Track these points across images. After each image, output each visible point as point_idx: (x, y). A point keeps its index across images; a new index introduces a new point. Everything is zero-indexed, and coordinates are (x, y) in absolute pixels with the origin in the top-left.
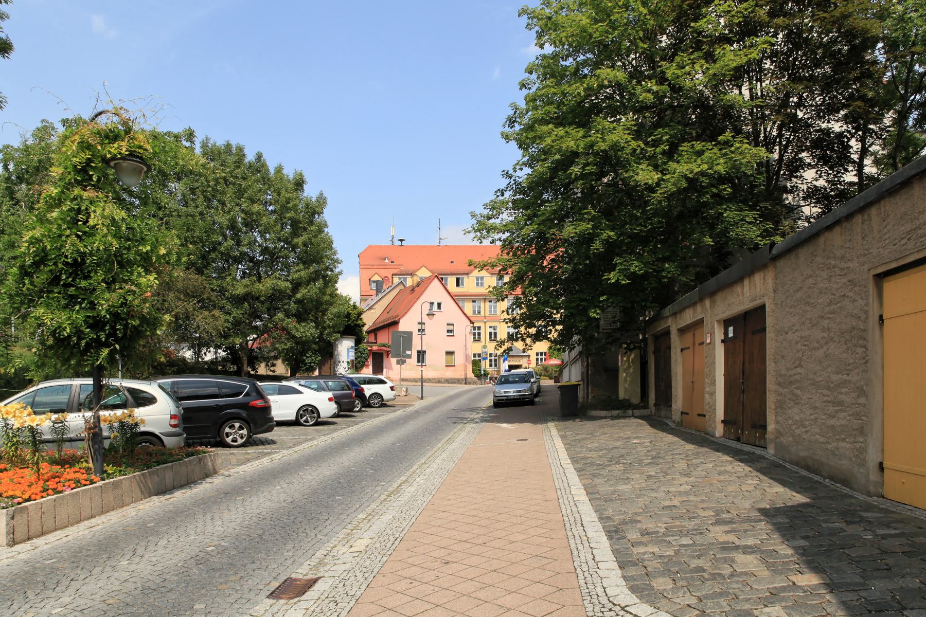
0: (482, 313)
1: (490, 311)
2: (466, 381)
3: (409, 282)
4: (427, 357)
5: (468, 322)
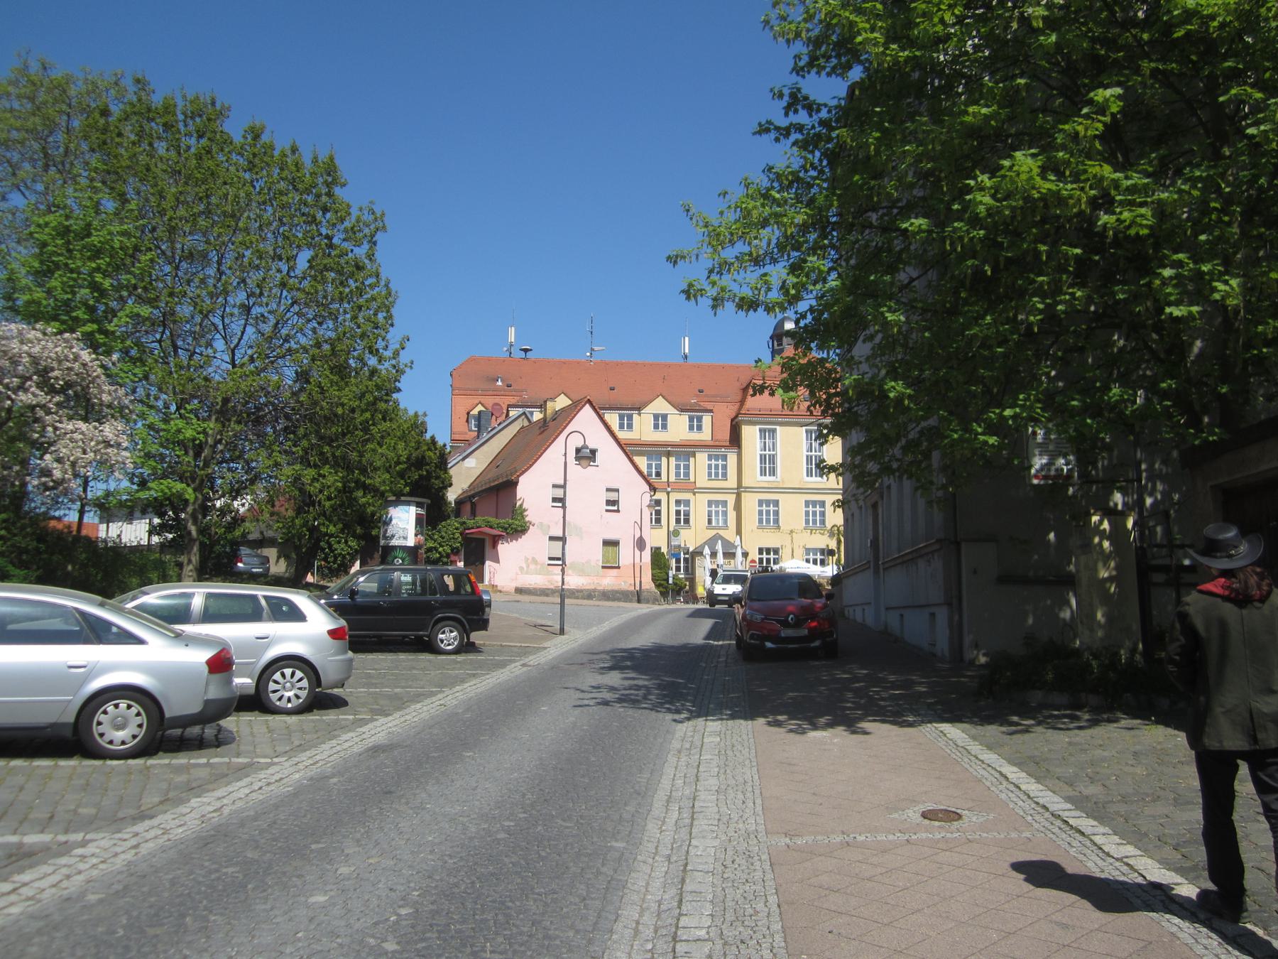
0: (664, 478)
1: (678, 474)
2: (639, 597)
3: (537, 416)
4: (611, 536)
5: (647, 488)
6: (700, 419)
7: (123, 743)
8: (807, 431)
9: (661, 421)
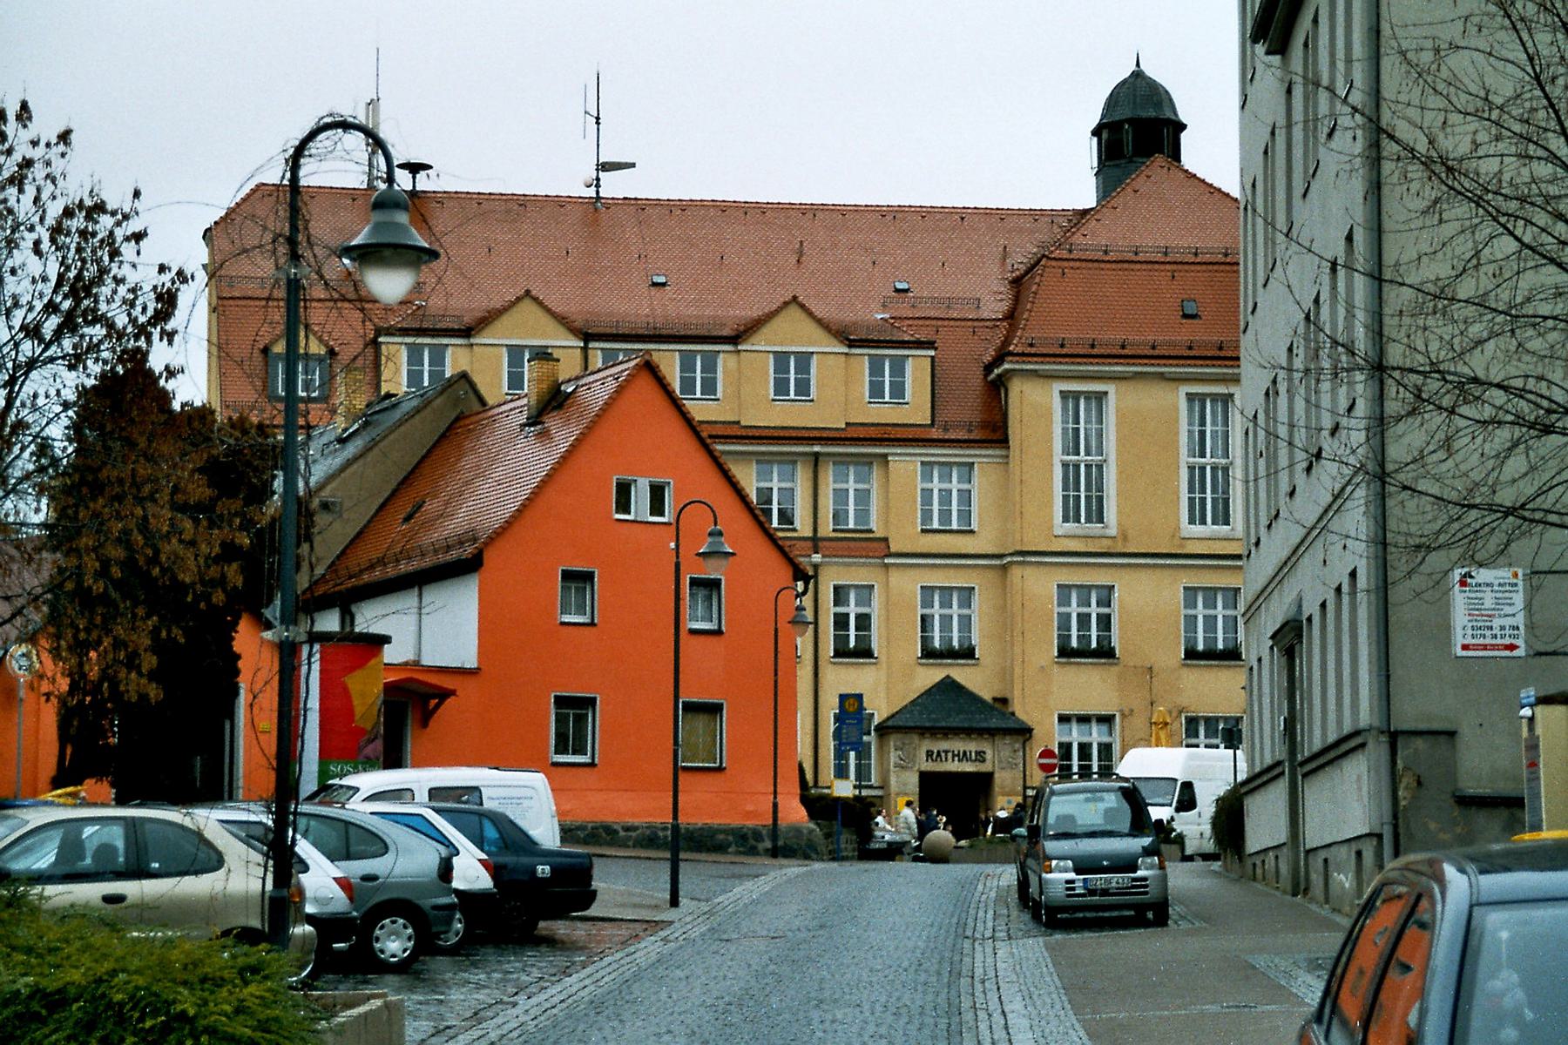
6: (898, 368)
7: (394, 956)
8: (1191, 397)
9: (792, 373)
